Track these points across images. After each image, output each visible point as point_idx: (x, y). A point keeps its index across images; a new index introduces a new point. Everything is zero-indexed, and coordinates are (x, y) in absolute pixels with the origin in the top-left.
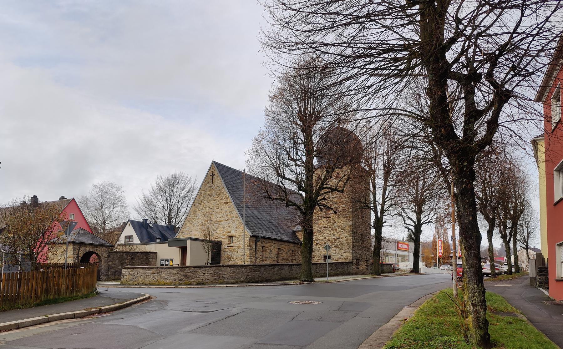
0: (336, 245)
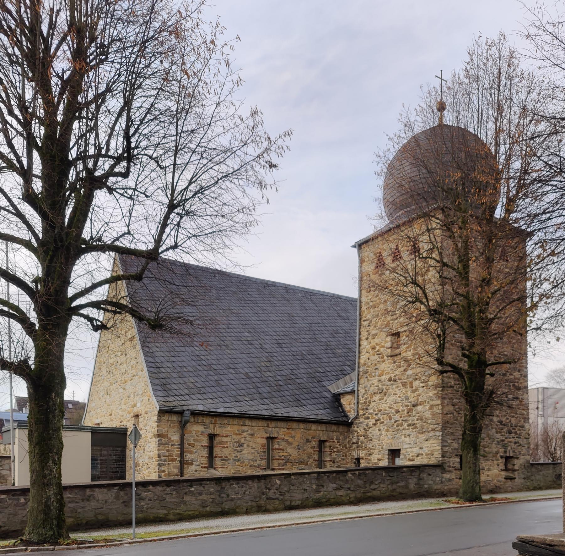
0: (410, 422)
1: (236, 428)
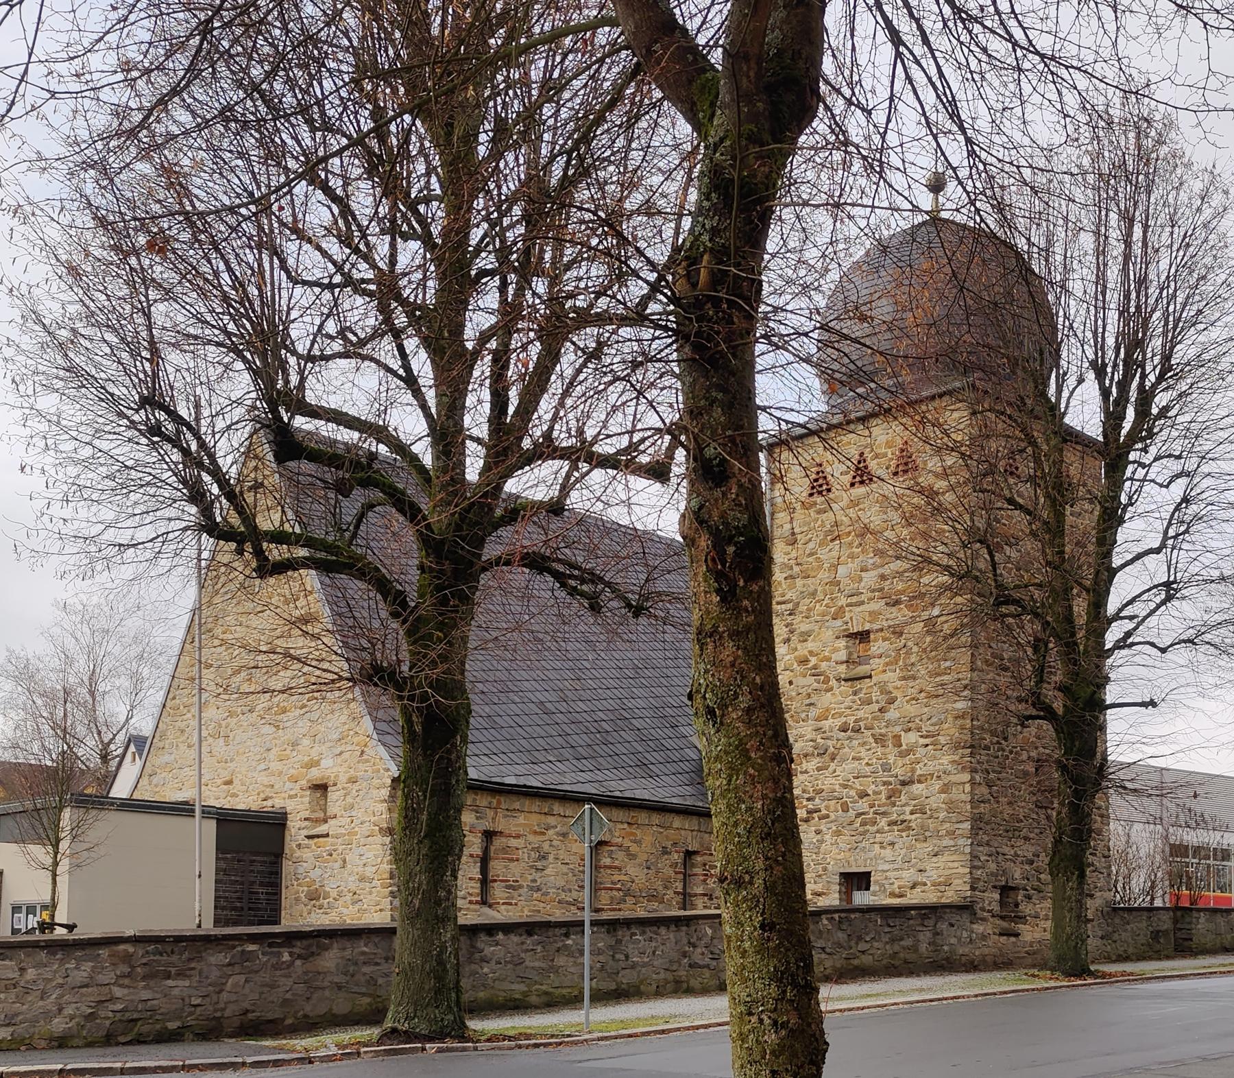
1: (534, 819)
